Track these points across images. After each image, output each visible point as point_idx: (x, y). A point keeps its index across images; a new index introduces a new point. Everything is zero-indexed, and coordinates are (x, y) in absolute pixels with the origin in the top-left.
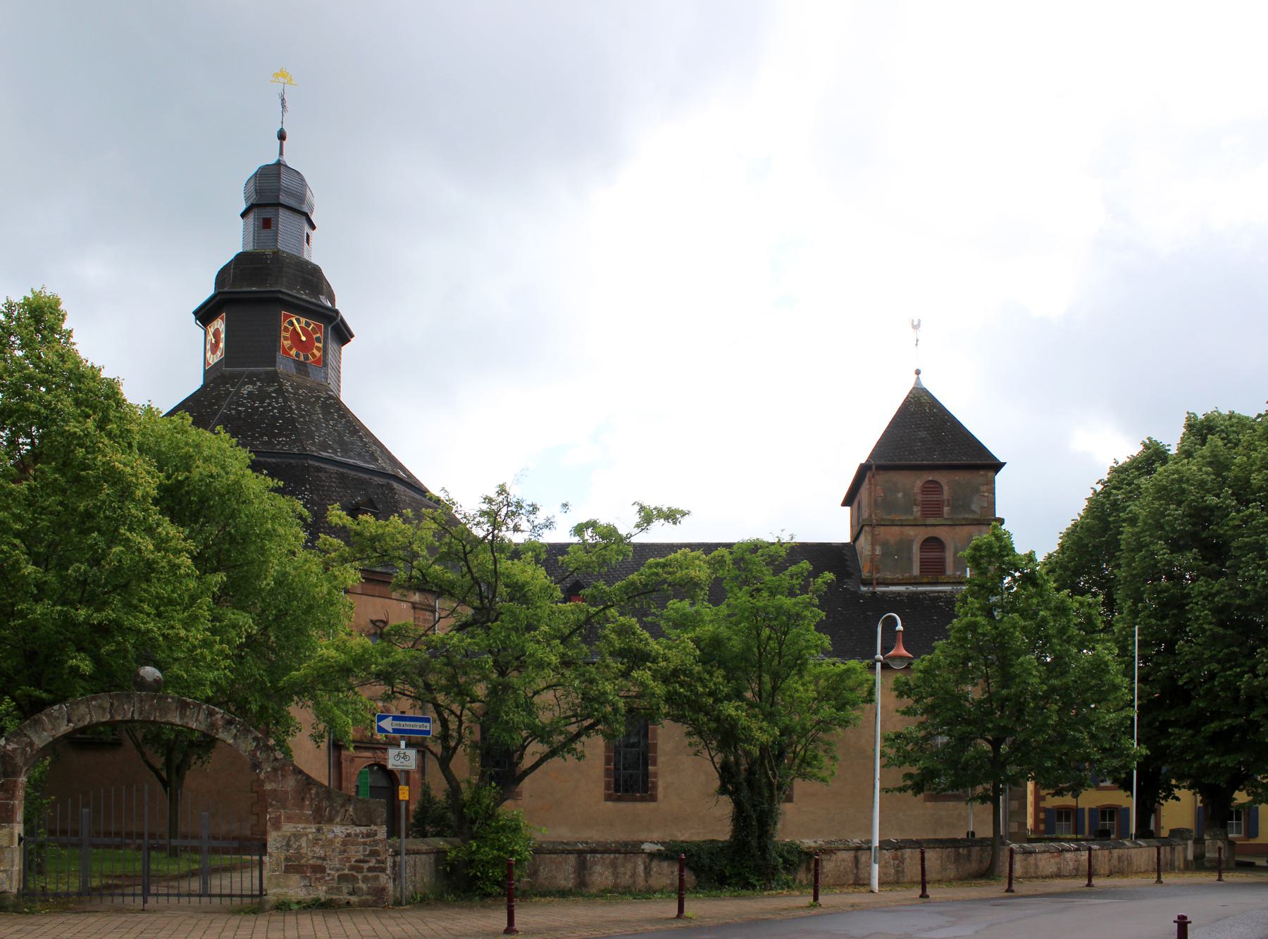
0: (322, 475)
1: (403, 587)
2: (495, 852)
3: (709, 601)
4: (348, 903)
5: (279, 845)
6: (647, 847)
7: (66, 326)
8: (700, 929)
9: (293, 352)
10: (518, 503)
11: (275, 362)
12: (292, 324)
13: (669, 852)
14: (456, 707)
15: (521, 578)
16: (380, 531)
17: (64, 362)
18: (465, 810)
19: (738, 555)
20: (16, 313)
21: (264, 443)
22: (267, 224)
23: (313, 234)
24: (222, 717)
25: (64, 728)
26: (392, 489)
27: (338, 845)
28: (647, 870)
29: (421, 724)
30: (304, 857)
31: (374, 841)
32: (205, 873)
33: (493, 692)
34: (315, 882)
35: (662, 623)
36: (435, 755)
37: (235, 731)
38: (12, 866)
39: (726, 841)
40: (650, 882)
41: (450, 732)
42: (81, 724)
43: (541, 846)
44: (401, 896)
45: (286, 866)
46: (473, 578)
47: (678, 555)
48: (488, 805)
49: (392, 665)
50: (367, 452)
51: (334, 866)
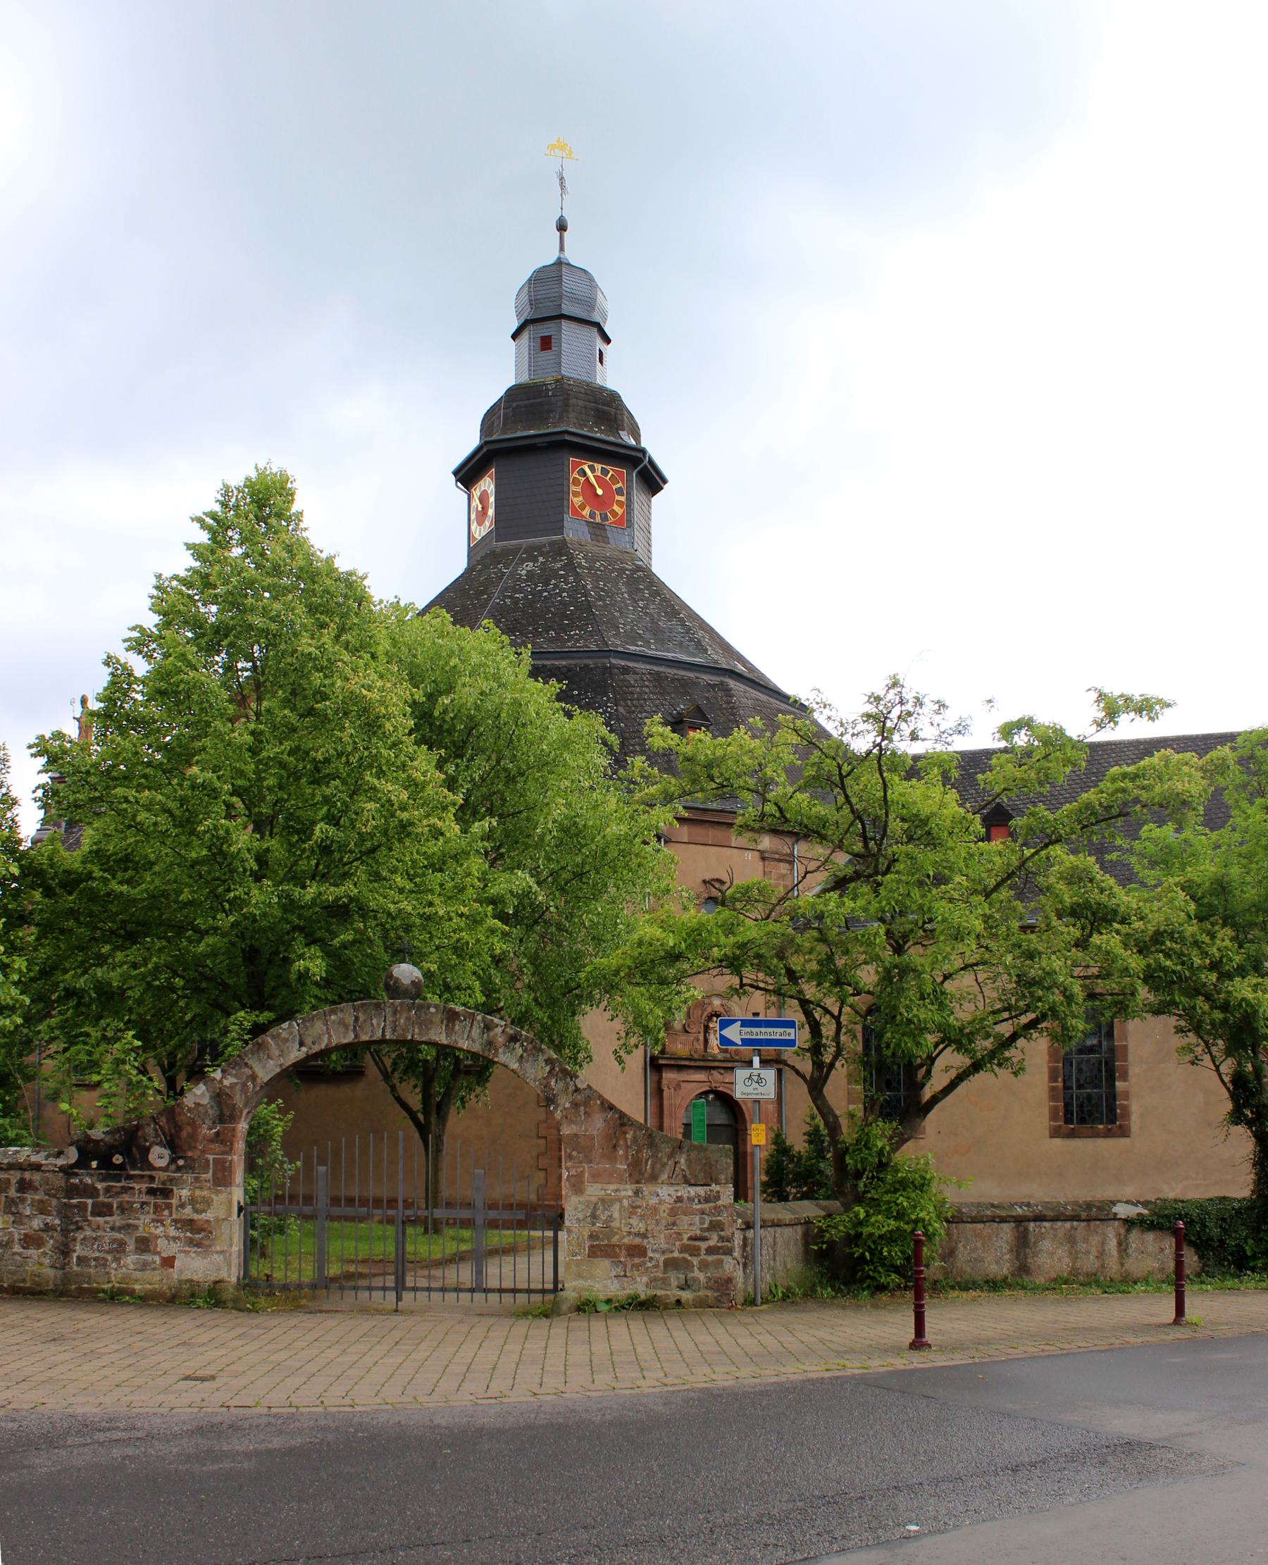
0: (631, 678)
1: (753, 830)
2: (892, 1222)
3: (1204, 824)
4: (678, 1302)
5: (581, 1216)
6: (1122, 1210)
7: (295, 508)
8: (1212, 1342)
9: (586, 512)
10: (917, 699)
11: (562, 527)
12: (584, 473)
13: (1155, 1218)
14: (831, 1003)
15: (925, 809)
16: (719, 752)
17: (293, 557)
18: (847, 1158)
19: (1245, 752)
20: (233, 500)
21: (551, 640)
22: (546, 343)
23: (608, 350)
24: (503, 1031)
25: (295, 1054)
26: (727, 691)
27: (663, 1214)
28: (1123, 1246)
29: (782, 1030)
30: (617, 1233)
31: (715, 1208)
32: (479, 1257)
33: (886, 977)
34: (632, 1270)
35: (1133, 860)
36: (803, 1077)
37: (520, 1051)
38: (231, 1245)
39: (1244, 1199)
40: (1126, 1266)
41: (824, 1041)
42: (316, 1048)
43: (959, 1211)
44: (755, 1293)
45: (592, 1246)
46: (853, 811)
47: (1156, 759)
48: (883, 1148)
49: (742, 946)
50: (691, 640)
51: (659, 1245)
